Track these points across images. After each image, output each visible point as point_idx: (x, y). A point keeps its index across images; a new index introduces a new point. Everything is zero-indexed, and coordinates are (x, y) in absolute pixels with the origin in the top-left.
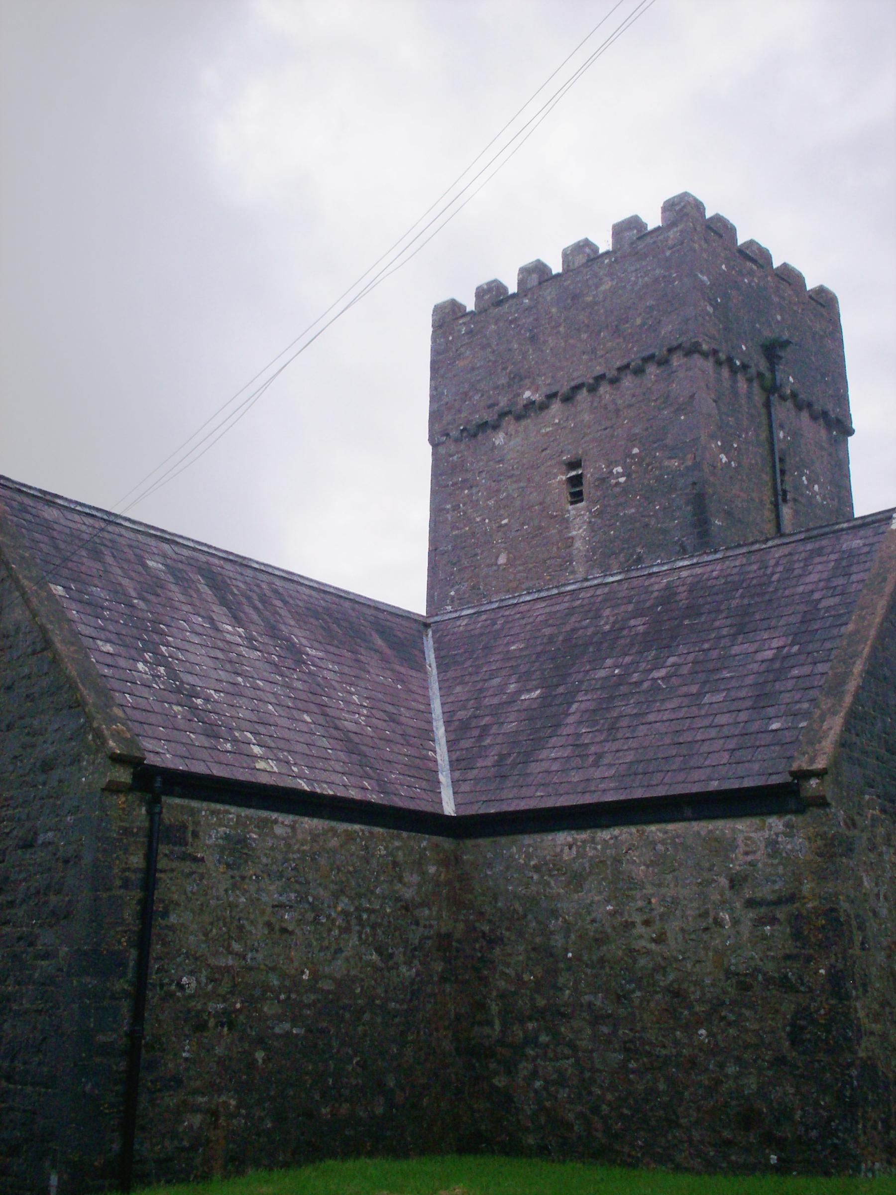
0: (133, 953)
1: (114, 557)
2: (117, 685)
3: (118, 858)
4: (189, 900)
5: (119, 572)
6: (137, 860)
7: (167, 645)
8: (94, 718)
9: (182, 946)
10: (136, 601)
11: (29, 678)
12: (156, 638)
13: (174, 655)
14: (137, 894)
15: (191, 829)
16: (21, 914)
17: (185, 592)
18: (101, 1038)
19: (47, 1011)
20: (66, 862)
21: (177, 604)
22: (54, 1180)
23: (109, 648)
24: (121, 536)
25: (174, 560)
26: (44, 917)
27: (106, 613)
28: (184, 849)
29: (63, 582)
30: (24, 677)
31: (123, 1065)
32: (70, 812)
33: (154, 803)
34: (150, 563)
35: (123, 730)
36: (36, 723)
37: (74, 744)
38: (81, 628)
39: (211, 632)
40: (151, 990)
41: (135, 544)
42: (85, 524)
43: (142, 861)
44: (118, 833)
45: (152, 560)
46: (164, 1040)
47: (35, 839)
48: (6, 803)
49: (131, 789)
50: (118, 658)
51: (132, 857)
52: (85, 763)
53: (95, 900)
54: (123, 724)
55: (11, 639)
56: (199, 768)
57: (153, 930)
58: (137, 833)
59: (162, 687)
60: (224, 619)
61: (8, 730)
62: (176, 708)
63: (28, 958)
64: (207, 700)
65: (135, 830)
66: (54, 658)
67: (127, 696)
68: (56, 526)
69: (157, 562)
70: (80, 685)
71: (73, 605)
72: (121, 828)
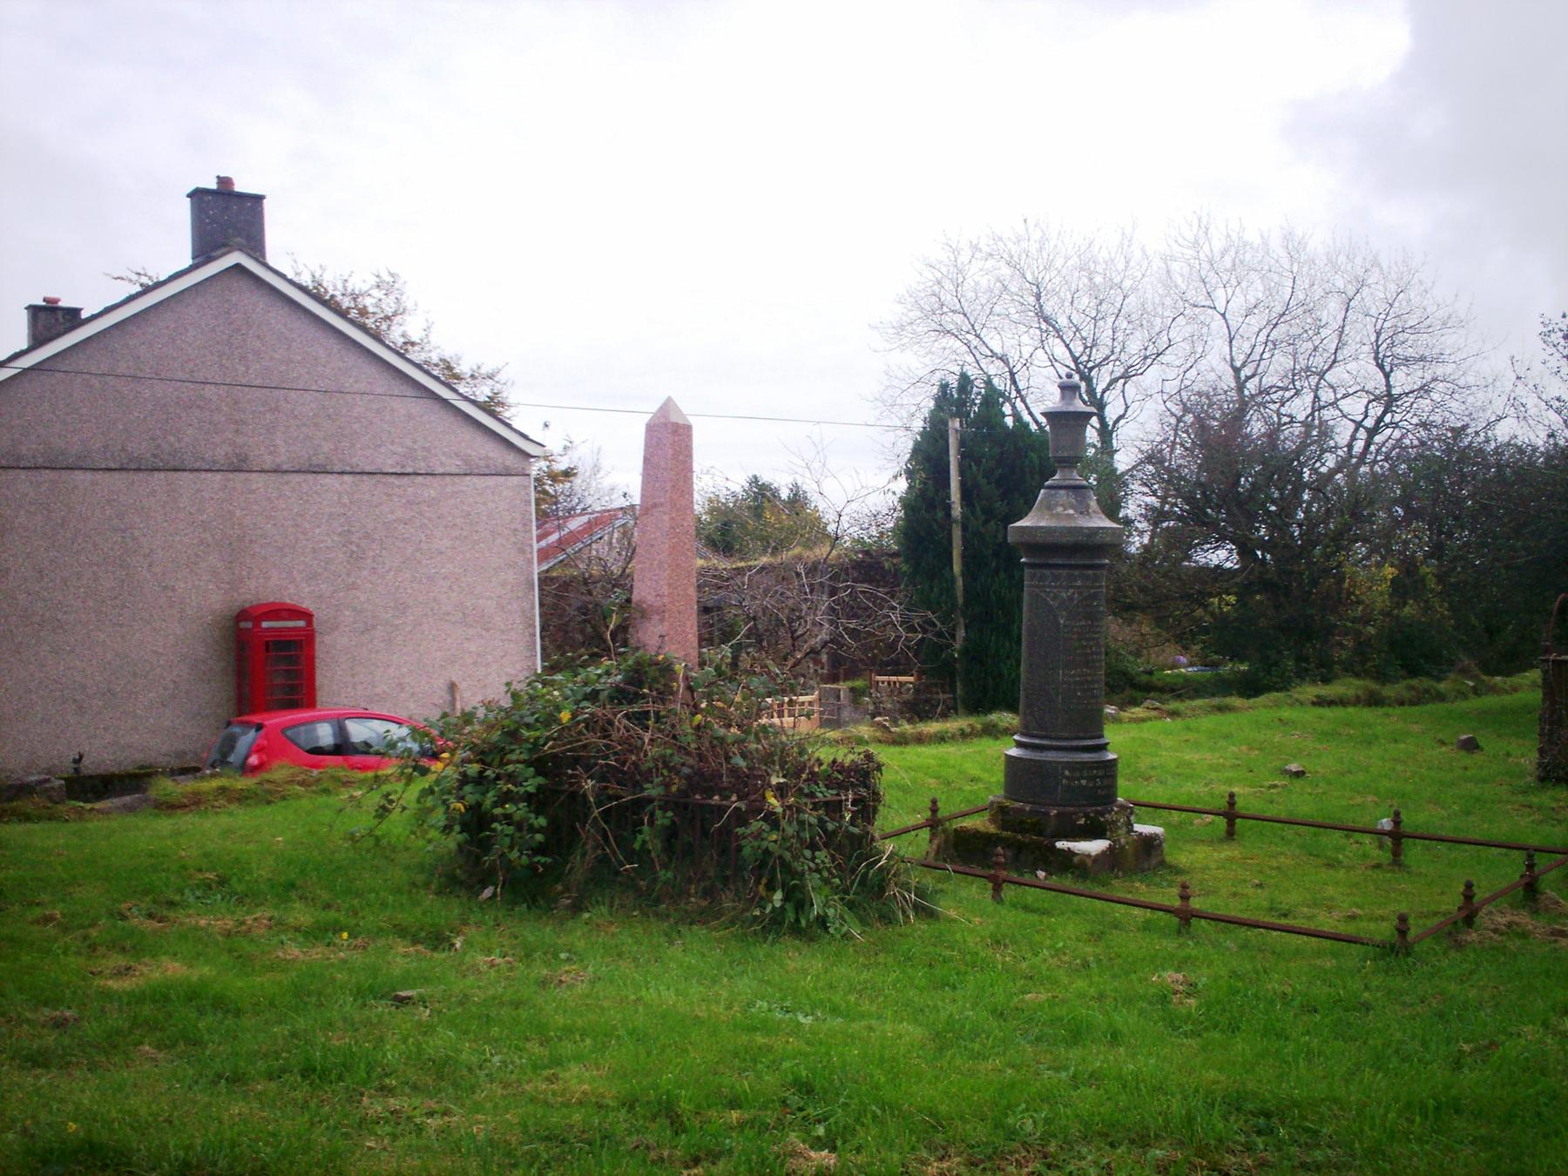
36: (676, 759)
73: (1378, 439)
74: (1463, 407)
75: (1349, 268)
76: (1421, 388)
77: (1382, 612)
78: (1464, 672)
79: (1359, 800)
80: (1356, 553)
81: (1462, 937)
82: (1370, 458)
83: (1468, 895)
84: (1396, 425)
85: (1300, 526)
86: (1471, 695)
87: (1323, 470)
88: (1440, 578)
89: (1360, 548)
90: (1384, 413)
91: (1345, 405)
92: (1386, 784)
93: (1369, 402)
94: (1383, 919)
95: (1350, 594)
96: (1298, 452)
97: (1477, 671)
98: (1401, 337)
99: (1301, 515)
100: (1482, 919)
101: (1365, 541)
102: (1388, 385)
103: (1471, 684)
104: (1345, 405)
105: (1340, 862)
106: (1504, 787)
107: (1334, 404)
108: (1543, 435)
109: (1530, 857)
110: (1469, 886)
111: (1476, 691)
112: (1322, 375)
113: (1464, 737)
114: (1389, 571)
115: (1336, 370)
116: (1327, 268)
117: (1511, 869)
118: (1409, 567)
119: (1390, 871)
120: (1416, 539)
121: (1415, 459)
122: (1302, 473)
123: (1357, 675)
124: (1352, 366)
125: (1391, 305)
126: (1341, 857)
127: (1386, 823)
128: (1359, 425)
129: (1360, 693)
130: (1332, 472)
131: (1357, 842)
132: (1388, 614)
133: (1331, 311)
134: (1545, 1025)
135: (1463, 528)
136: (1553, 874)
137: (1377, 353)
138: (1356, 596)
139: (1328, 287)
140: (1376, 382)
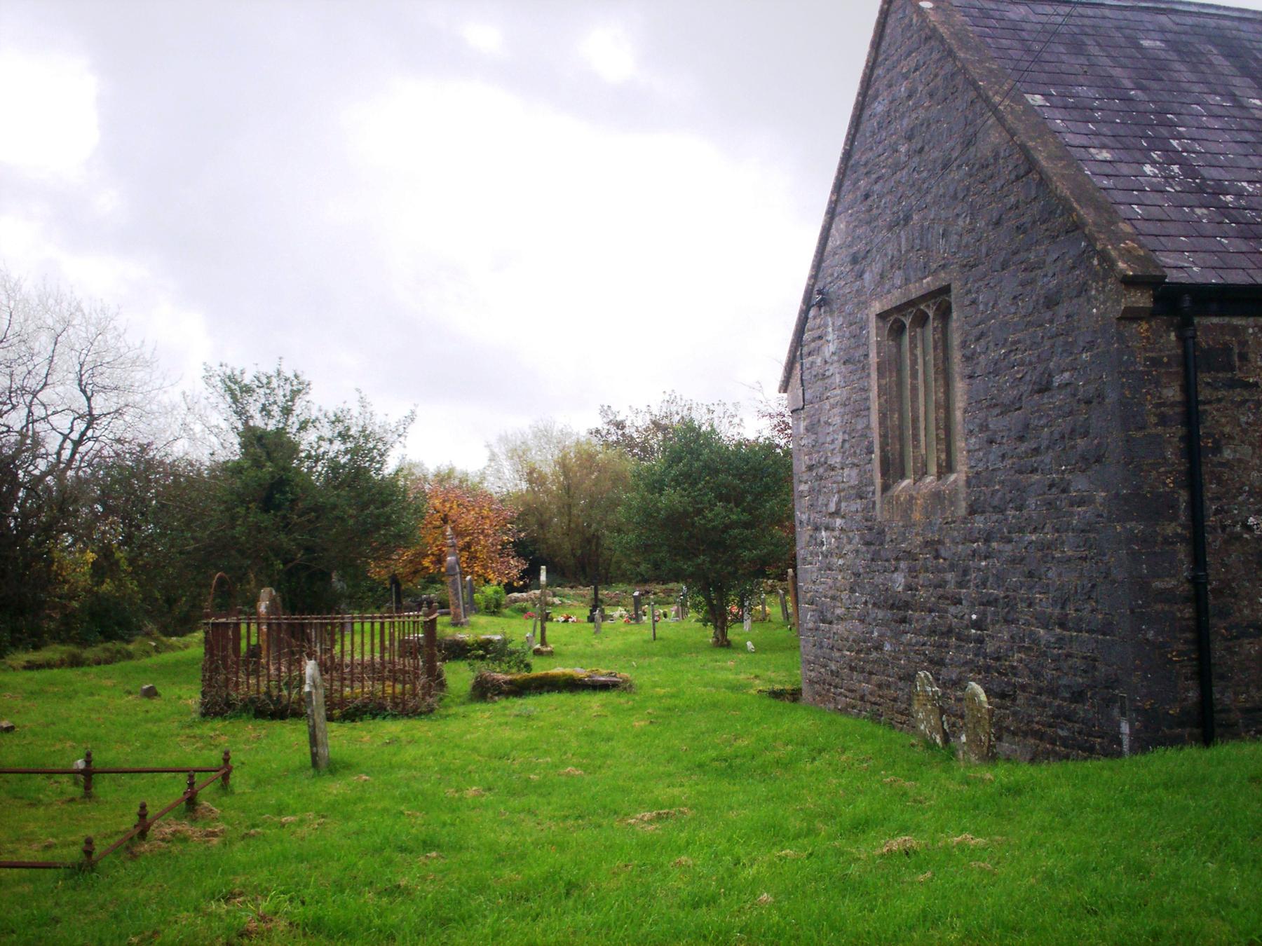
0: (1183, 497)
1: (1099, 45)
2: (1119, 196)
3: (1148, 393)
4: (1244, 431)
5: (1107, 61)
6: (1172, 393)
7: (1179, 137)
8: (1096, 240)
9: (1244, 484)
10: (1132, 92)
11: (1017, 208)
12: (1164, 132)
13: (1189, 148)
14: (1179, 430)
15: (1236, 351)
16: (1047, 460)
17: (1194, 70)
18: (1158, 584)
19: (1092, 558)
20: (1089, 402)
21: (1186, 86)
22: (1125, 728)
23: (1105, 155)
24: (1104, 18)
25: (1175, 33)
26: (1074, 462)
27: (1098, 114)
28: (1229, 375)
29: (1042, 88)
30: (1011, 208)
31: (1188, 612)
32: (1084, 349)
33: (1184, 327)
34: (1146, 43)
35: (1133, 247)
36: (1032, 257)
37: (1078, 272)
38: (1069, 138)
39: (1236, 112)
40: (1210, 533)
41: (1124, 23)
42: (1058, 14)
43: (1178, 393)
44: (1145, 365)
45: (1146, 39)
46: (1234, 585)
47: (1050, 382)
48: (1014, 348)
49: (1152, 314)
50: (1119, 165)
51: (1165, 391)
52: (1093, 292)
53: (1128, 441)
54: (1133, 241)
55: (991, 167)
56: (1237, 278)
57: (1204, 468)
58: (1168, 363)
59: (1178, 189)
60: (1250, 92)
61: (1003, 269)
62: (1198, 211)
63: (1063, 504)
64: (1239, 194)
65: (1165, 360)
66: (1041, 179)
67: (1135, 207)
68: (1024, 25)
69: (1155, 40)
70: (1075, 205)
71: (1057, 113)
72: (1147, 359)
73: (81, 449)
74: (149, 428)
75: (57, 310)
76: (116, 411)
77: (84, 589)
78: (148, 634)
79: (59, 746)
80: (63, 541)
81: (135, 849)
82: (75, 464)
83: (142, 814)
84: (96, 439)
85: (15, 518)
86: (154, 653)
87: (36, 472)
88: (131, 562)
89: (66, 537)
90: (87, 429)
91: (54, 420)
92: (83, 730)
93: (75, 419)
94: (74, 843)
95: (57, 575)
96: (14, 457)
97: (156, 633)
98: (100, 369)
99: (16, 509)
100: (153, 832)
101: (71, 531)
102: (90, 407)
103: (154, 644)
104: (54, 420)
105: (40, 801)
106: (176, 724)
107: (45, 419)
108: (207, 452)
109: (191, 777)
110: (143, 807)
111: (157, 650)
112: (35, 394)
113: (146, 687)
114: (90, 556)
115: (47, 390)
116: (39, 308)
117: (176, 788)
118: (106, 553)
119: (81, 804)
120: (112, 531)
121: (112, 467)
122: (17, 475)
123: (63, 642)
124: (60, 389)
125: (92, 344)
126: (41, 796)
127: (80, 764)
128: (66, 437)
129: (64, 656)
130: (44, 474)
131: (56, 782)
132: (89, 591)
133: (42, 343)
134: (196, 909)
135: (147, 522)
136: (208, 789)
137: (81, 381)
138: (63, 577)
139: (39, 323)
140: (81, 404)
